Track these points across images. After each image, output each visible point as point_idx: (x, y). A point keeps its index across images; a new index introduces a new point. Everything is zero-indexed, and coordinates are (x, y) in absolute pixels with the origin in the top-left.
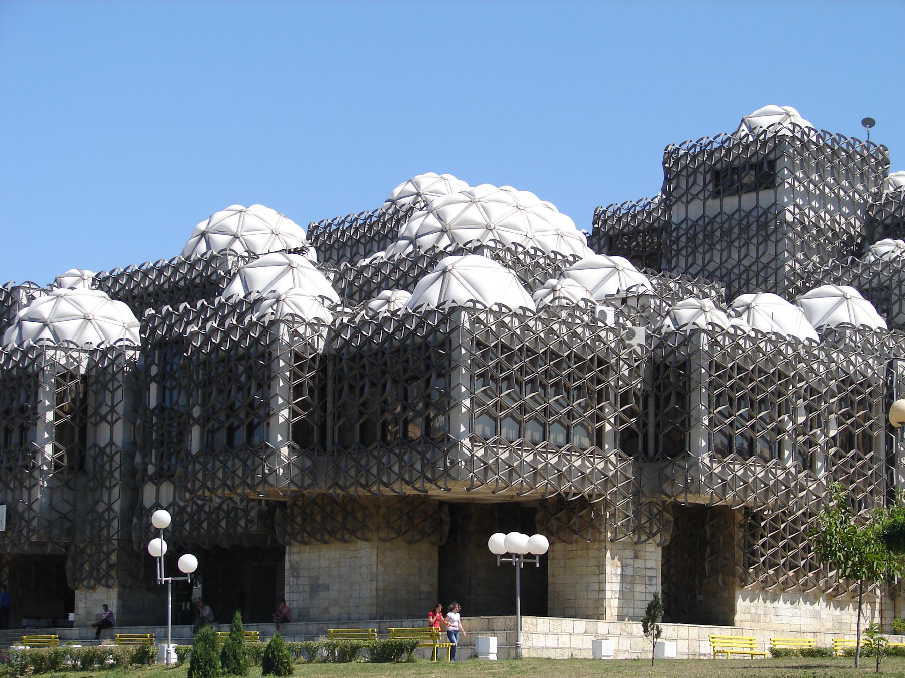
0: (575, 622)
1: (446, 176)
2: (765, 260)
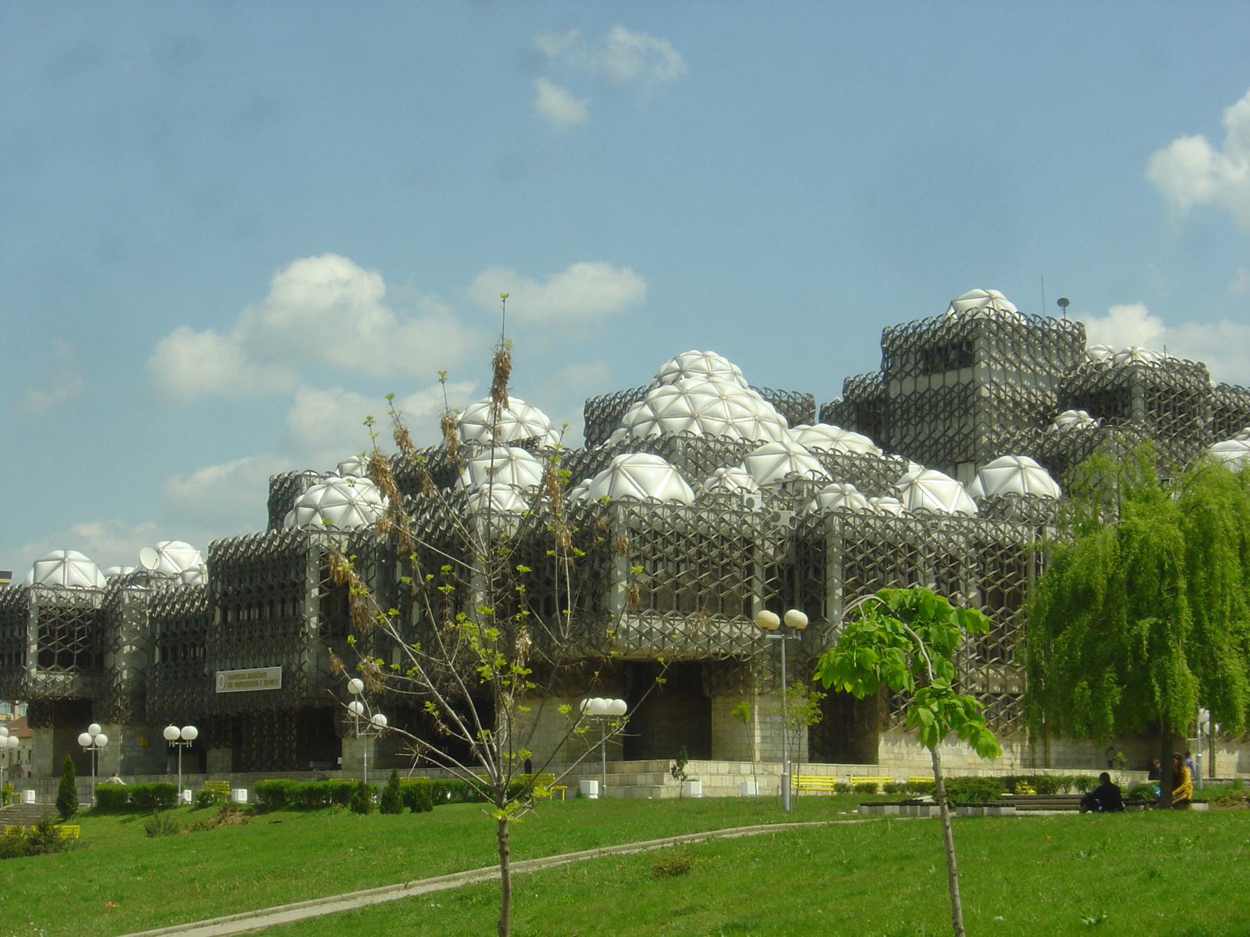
0: (720, 765)
1: (710, 353)
2: (965, 431)
